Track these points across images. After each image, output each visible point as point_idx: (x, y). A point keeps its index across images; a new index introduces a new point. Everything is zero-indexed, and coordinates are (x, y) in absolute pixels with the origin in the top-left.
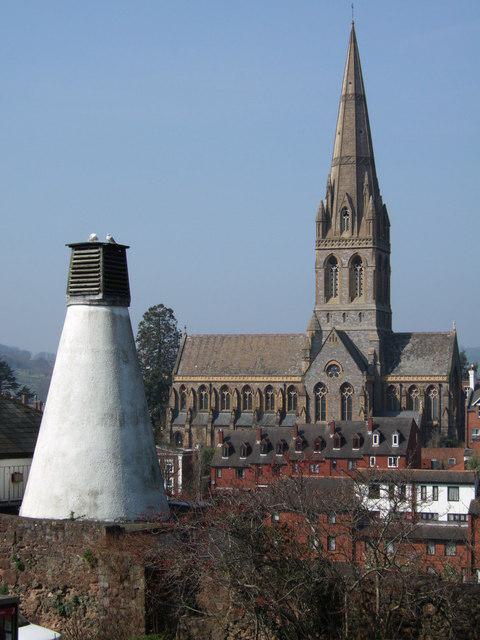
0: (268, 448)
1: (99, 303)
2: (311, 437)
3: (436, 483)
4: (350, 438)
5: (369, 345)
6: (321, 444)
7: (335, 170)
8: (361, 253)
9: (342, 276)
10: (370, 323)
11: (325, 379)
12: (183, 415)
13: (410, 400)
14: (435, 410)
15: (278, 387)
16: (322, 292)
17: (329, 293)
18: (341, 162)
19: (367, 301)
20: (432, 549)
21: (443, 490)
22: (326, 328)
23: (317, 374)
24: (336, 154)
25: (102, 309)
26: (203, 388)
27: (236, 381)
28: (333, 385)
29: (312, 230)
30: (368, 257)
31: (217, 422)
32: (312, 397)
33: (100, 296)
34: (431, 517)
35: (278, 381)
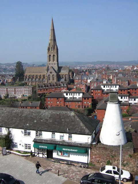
0: (45, 86)
1: (117, 104)
2: (52, 84)
3: (76, 93)
4: (58, 85)
5: (56, 69)
6: (54, 86)
7: (50, 41)
8: (55, 54)
9: (52, 58)
10: (56, 65)
11: (50, 74)
12: (27, 80)
13: (63, 77)
14: (66, 78)
15: (42, 75)
16: (48, 60)
17: (50, 61)
18: (51, 40)
19: (55, 62)
20: (61, 99)
21: (78, 94)
22: (49, 66)
23: (49, 73)
24: (50, 39)
25: (118, 105)
26: (30, 75)
27: (35, 74)
28: (51, 75)
29: (47, 51)
30: (56, 55)
31: (32, 81)
32: (48, 77)
33: (117, 102)
34: (76, 98)
35: (42, 74)
